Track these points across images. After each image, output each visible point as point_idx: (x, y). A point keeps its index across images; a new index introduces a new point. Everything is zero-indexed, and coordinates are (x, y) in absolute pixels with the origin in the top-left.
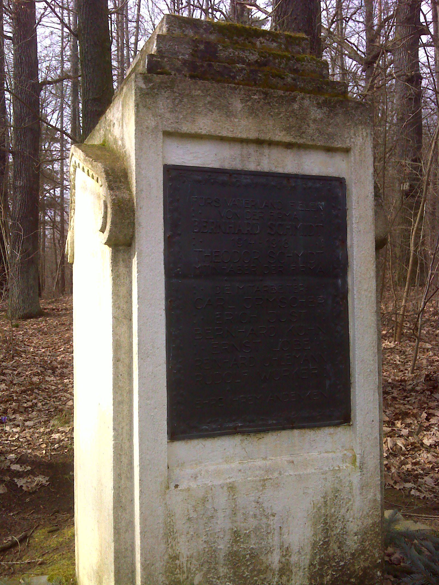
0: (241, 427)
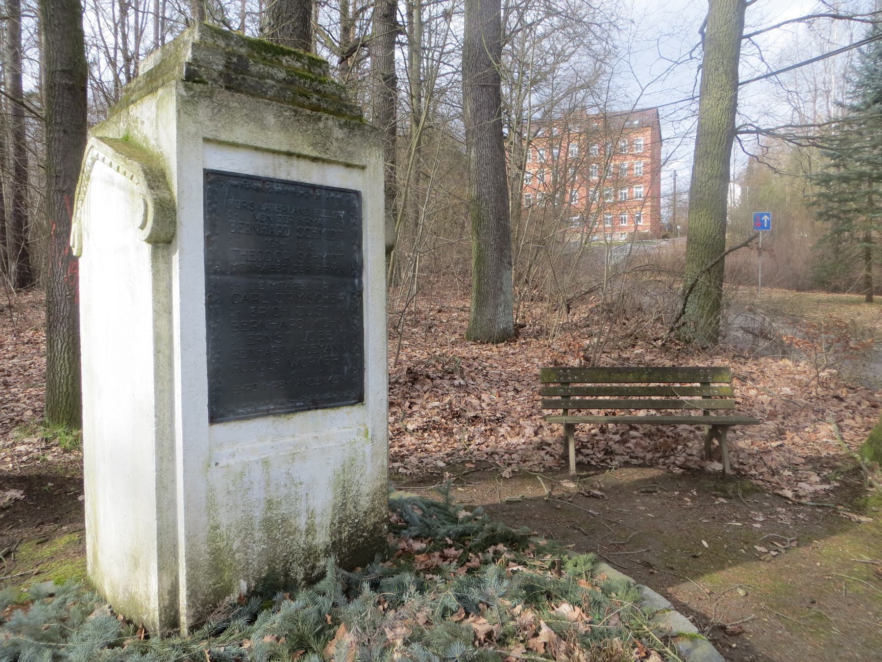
0: (273, 409)
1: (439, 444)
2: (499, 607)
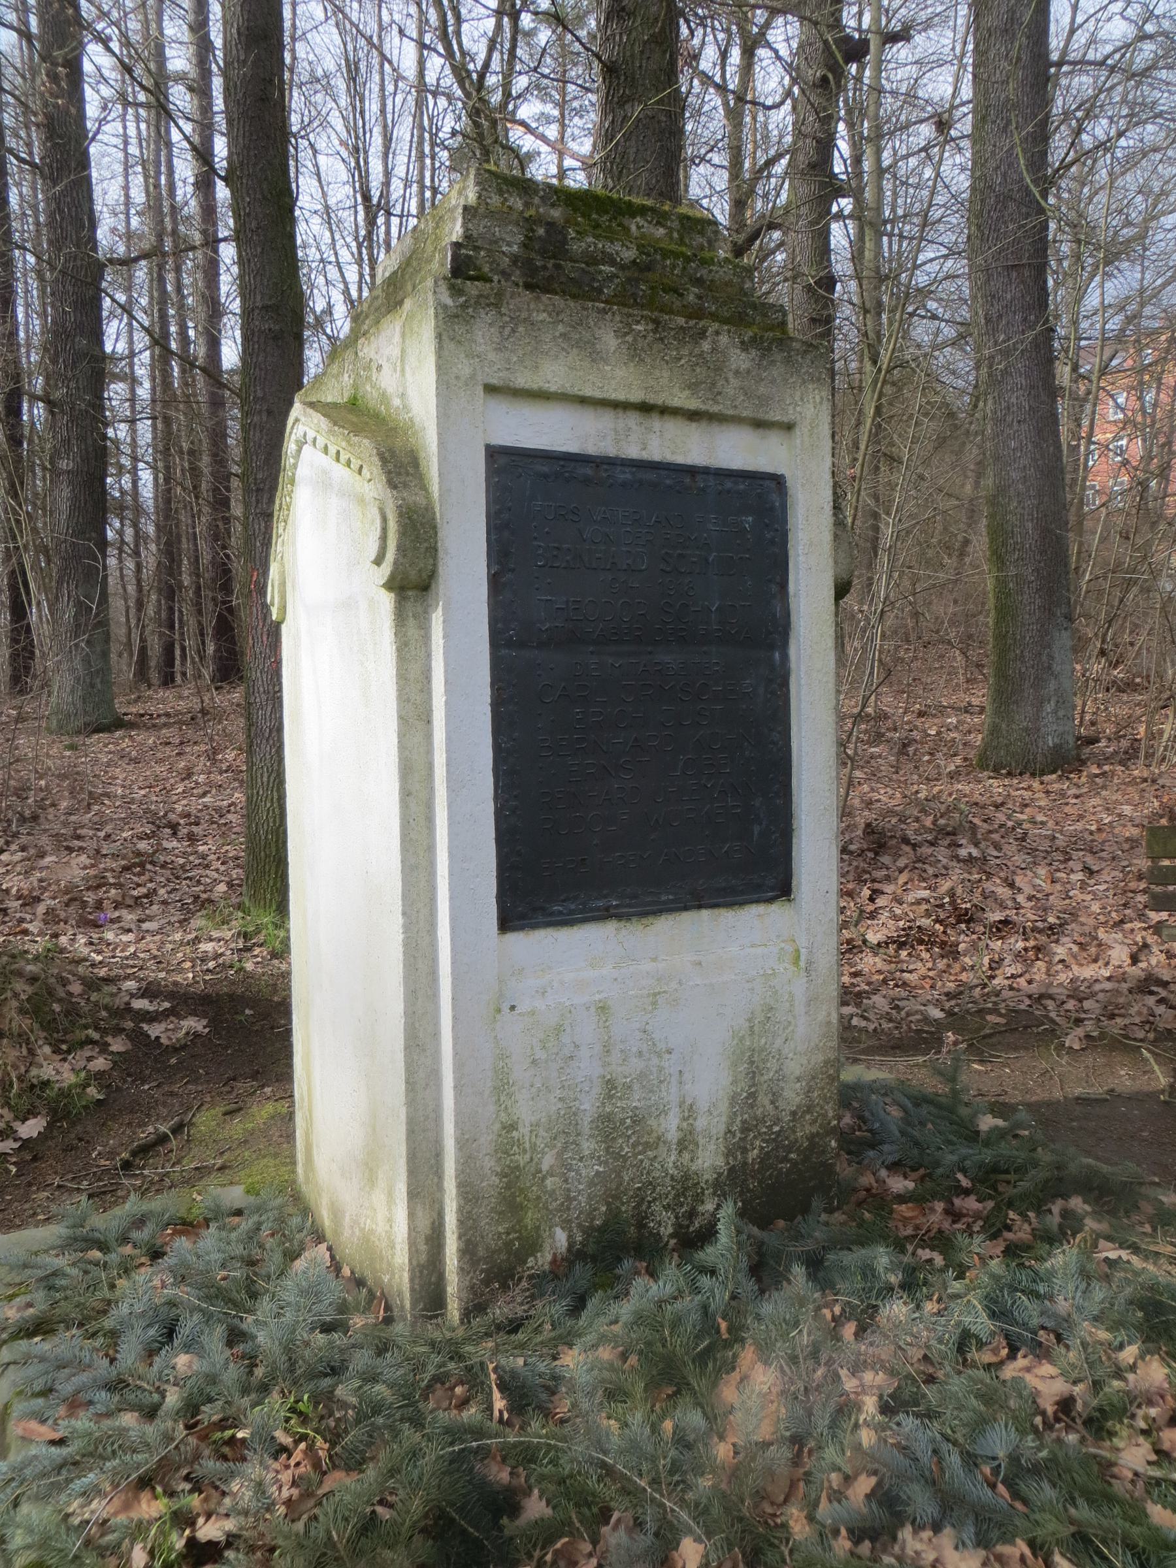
0: (617, 906)
1: (931, 974)
2: (1084, 1345)
